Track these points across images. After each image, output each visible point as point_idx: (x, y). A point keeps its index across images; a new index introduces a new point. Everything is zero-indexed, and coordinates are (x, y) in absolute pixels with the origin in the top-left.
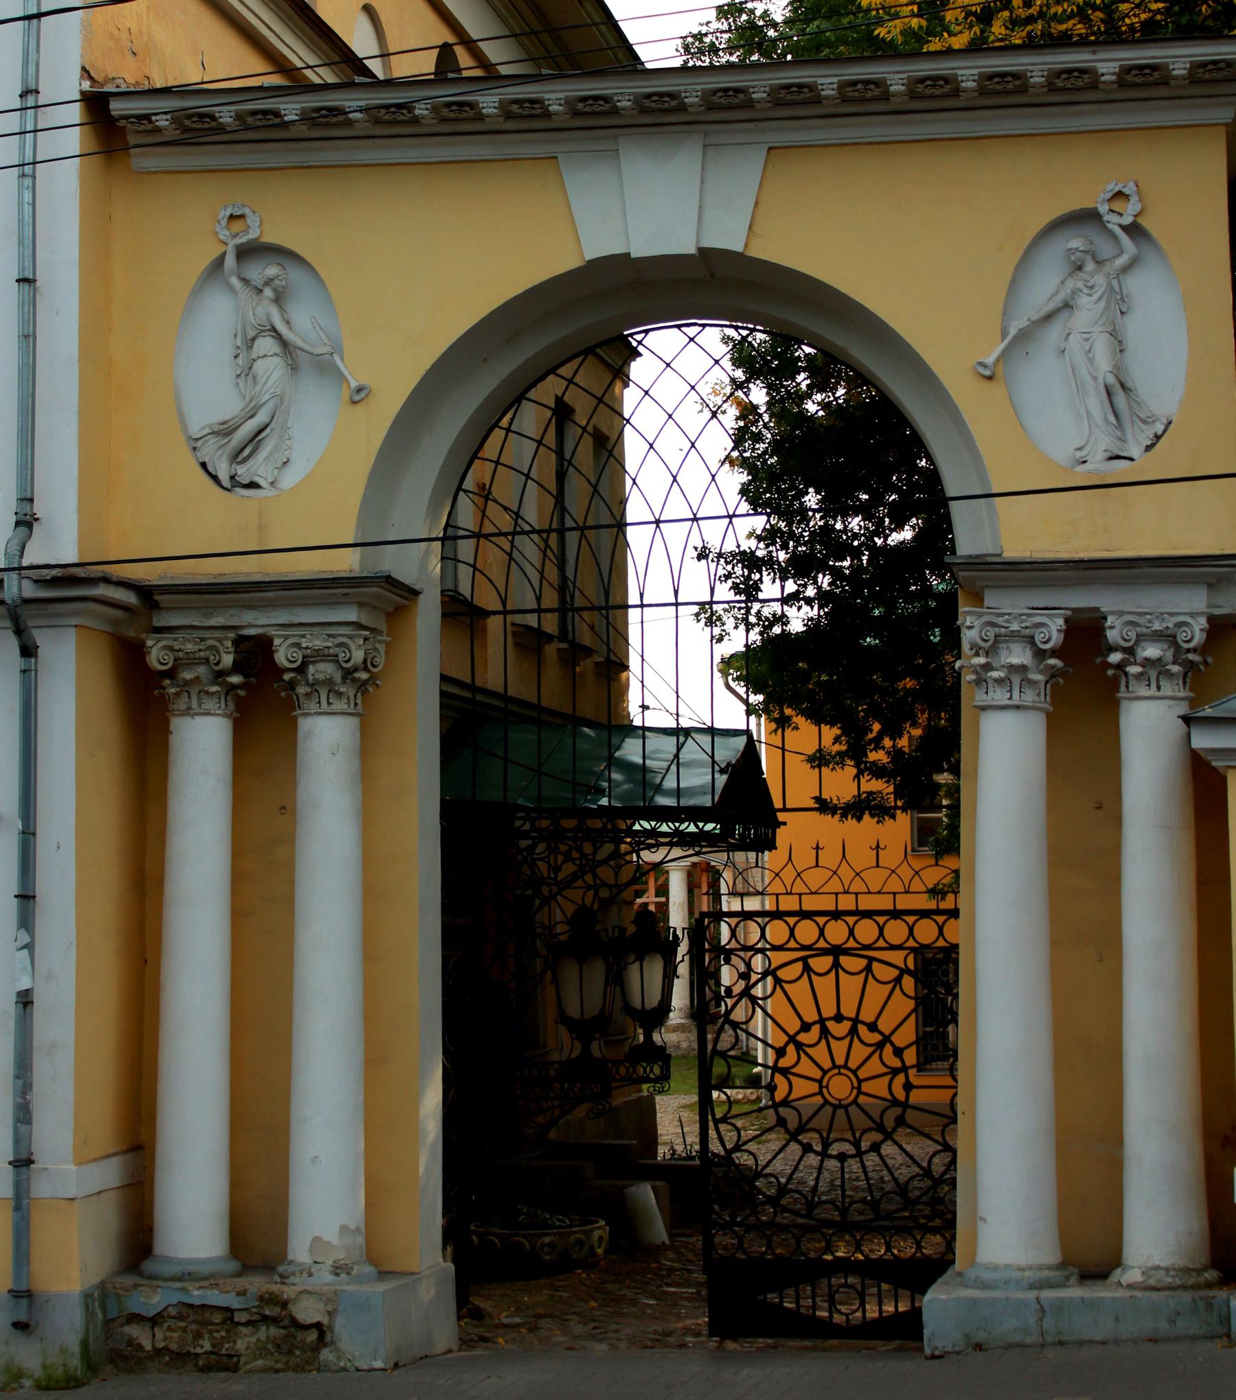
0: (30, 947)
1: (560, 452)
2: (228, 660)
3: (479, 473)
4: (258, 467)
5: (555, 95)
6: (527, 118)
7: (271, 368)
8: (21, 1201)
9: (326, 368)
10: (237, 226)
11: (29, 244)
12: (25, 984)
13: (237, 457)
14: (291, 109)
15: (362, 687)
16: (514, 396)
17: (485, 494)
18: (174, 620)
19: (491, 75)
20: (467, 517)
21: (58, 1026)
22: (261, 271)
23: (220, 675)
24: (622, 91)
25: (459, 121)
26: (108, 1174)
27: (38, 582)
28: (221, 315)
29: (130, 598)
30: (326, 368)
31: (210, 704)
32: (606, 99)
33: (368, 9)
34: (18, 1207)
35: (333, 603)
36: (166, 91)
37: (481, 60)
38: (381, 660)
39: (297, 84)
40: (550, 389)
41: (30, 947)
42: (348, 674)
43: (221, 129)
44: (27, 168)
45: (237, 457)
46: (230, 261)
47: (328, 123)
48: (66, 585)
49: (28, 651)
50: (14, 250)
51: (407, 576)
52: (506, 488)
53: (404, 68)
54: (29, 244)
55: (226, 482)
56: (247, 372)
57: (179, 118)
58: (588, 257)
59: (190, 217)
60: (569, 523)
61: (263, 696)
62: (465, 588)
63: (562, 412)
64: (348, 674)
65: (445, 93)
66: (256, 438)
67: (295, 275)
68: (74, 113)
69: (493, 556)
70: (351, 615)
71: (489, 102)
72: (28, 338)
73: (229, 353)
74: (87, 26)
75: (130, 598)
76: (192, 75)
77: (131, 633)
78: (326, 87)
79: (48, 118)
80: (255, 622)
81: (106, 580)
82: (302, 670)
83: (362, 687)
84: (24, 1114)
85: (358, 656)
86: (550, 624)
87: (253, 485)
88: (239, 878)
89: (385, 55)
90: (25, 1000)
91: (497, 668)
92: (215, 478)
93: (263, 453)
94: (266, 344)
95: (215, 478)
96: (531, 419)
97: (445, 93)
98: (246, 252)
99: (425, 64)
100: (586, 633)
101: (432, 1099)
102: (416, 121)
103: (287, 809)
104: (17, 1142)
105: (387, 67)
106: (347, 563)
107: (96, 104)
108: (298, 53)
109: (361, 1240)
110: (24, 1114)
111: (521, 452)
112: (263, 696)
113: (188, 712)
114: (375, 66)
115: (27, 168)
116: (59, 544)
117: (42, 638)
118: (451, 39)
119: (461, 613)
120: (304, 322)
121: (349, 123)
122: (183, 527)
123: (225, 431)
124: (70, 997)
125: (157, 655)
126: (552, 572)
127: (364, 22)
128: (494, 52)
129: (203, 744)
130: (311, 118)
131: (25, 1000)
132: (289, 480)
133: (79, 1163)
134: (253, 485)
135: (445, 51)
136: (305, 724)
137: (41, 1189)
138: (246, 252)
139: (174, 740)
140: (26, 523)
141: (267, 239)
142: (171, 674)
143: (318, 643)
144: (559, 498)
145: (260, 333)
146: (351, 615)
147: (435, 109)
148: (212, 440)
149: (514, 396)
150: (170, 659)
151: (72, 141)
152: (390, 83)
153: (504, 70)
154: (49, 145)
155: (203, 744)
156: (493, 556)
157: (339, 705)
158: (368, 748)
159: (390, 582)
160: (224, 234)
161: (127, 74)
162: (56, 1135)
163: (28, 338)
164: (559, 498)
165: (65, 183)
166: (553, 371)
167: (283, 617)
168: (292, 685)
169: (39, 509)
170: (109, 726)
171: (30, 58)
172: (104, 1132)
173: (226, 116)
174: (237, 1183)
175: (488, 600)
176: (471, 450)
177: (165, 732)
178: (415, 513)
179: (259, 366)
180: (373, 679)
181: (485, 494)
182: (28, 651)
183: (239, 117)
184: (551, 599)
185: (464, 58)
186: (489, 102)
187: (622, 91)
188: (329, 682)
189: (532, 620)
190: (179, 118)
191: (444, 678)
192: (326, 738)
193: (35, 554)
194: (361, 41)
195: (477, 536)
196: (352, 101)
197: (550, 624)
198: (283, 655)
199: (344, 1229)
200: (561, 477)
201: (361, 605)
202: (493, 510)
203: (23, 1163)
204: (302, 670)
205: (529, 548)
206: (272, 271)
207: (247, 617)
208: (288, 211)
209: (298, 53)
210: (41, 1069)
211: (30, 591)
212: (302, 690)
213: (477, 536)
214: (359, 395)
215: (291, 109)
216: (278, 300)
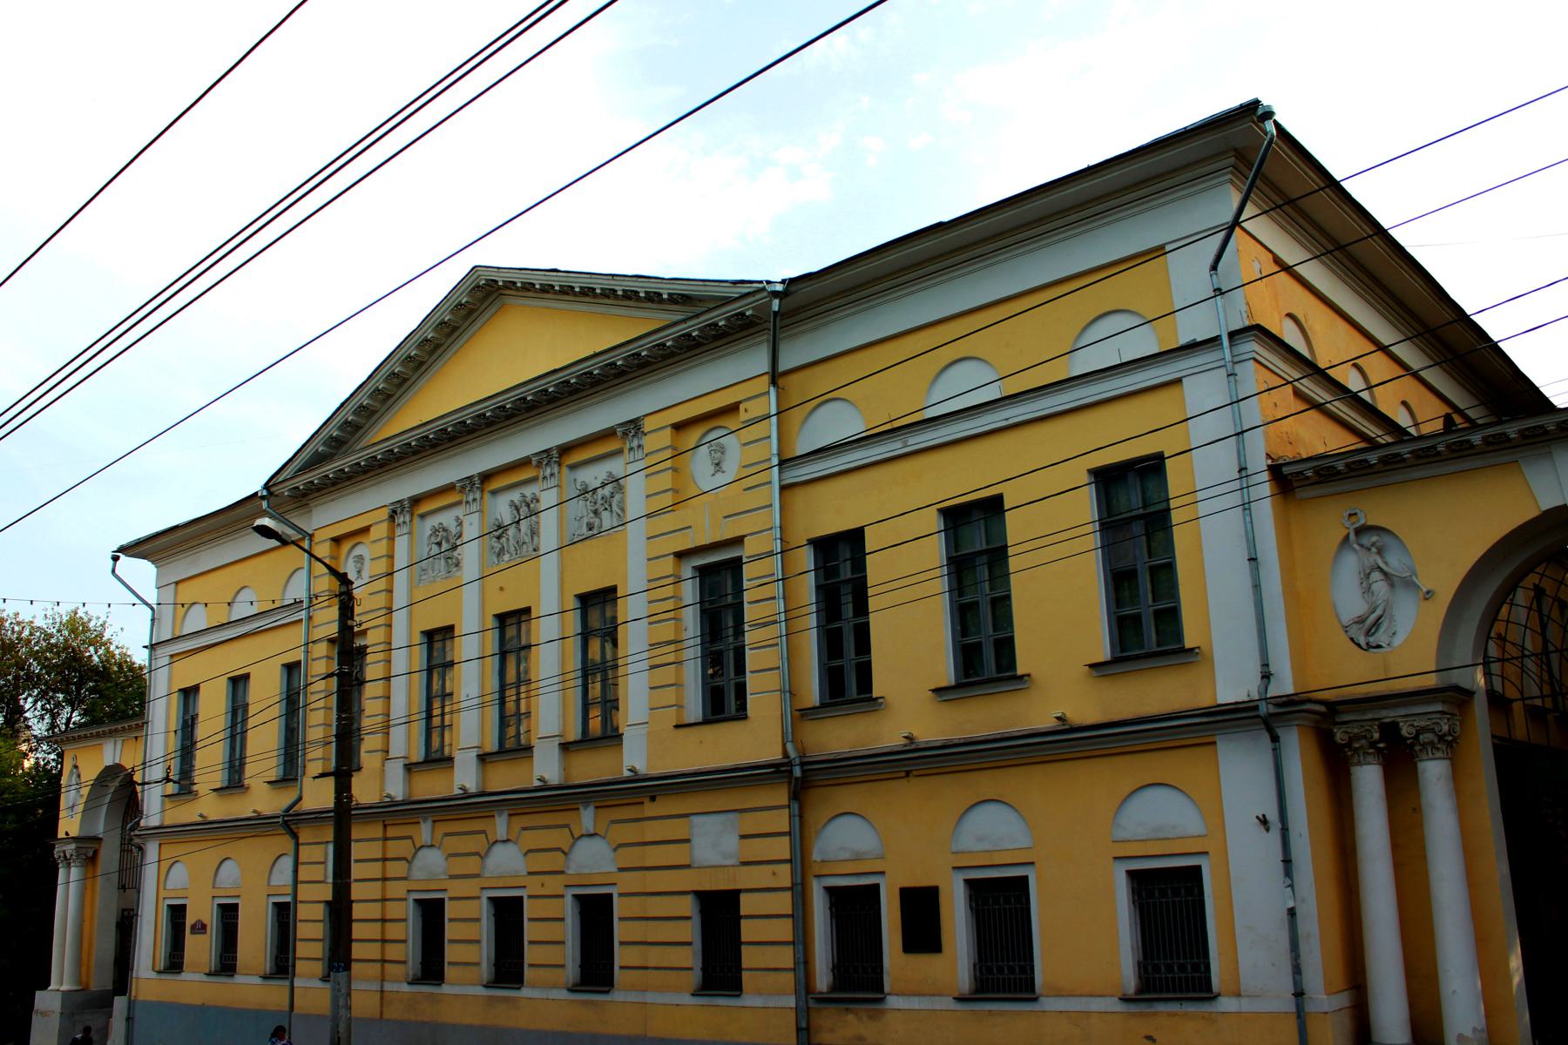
0: (1291, 886)
1: (1540, 611)
2: (1376, 736)
3: (1499, 627)
4: (1381, 637)
5: (1512, 430)
6: (1498, 444)
7: (1380, 587)
8: (1300, 1014)
9: (1409, 584)
10: (1353, 519)
11: (1251, 542)
12: (1291, 904)
13: (1368, 633)
14: (1373, 458)
15: (1449, 745)
16: (1505, 594)
17: (1502, 639)
18: (1347, 718)
19: (1473, 425)
20: (1493, 651)
21: (1310, 926)
22: (1367, 540)
23: (1373, 744)
24: (1549, 422)
25: (1462, 451)
26: (1343, 1000)
27: (1277, 705)
28: (1350, 565)
29: (1322, 709)
30: (1409, 584)
31: (1370, 759)
32: (1542, 427)
33: (1404, 403)
34: (1299, 1017)
35: (1428, 703)
36: (1310, 459)
37: (1467, 418)
38: (1458, 729)
39: (1373, 445)
40: (1532, 579)
41: (1291, 886)
42: (1441, 738)
43: (1339, 472)
44: (1246, 506)
45: (1368, 633)
46: (1352, 536)
47: (1392, 463)
48: (1290, 705)
49: (1275, 739)
50: (1245, 545)
51: (1467, 685)
52: (1514, 634)
53: (1426, 429)
54: (1251, 542)
55: (1363, 644)
56: (1368, 590)
57: (1317, 471)
58: (1544, 508)
59: (1328, 520)
60: (1551, 648)
61: (1399, 761)
62: (1498, 687)
63: (1539, 592)
64: (1441, 738)
65: (1452, 438)
66: (1377, 623)
67: (1386, 539)
68: (1265, 476)
69: (1511, 670)
70: (1439, 707)
71: (1476, 438)
72: (1257, 587)
73: (1356, 581)
74: (1266, 434)
75: (1322, 709)
76: (1321, 450)
77: (1324, 726)
78: (1388, 444)
79: (1253, 480)
80: (1388, 715)
81: (1310, 701)
82: (1416, 737)
83: (1450, 744)
84: (1297, 970)
85: (1446, 728)
86: (1549, 704)
87: (1379, 646)
88: (1396, 846)
89: (1416, 425)
90: (1292, 912)
91: (1521, 728)
92: (1359, 645)
93: (1382, 630)
94: (1376, 575)
95: (1359, 645)
96: (1521, 597)
97: (1452, 438)
98: (1360, 531)
99: (1438, 425)
100: (83, 879)
101: (1516, 963)
102: (1439, 453)
103: (1417, 810)
104: (1295, 983)
105: (1418, 430)
106: (1431, 681)
107: (1276, 471)
108: (1372, 430)
109: (1485, 1035)
110: (1297, 970)
111: (1521, 615)
112: (1399, 761)
113: (1359, 764)
114: (1412, 431)
115: (1246, 506)
116: (1285, 685)
117: (1280, 732)
118: (1449, 411)
119: (1497, 702)
120: (1394, 562)
121: (1404, 460)
122: (1346, 671)
123: (1361, 621)
124: (1315, 913)
125: (1340, 736)
126: (1546, 676)
127: (1403, 410)
128: (1471, 414)
129: (1369, 780)
130: (1384, 461)
131: (1292, 912)
132: (1397, 641)
133: (1328, 994)
134: (1379, 646)
135: (1448, 420)
136: (1422, 766)
137: (1310, 1007)
138: (1360, 531)
139: (1353, 778)
140: (1266, 676)
141: (1370, 523)
142: (1349, 745)
143: (1423, 724)
144: (1543, 634)
145: (1372, 570)
146: (1439, 707)
147: (1448, 446)
148: (1355, 627)
149: (1505, 594)
150: (1346, 737)
151: (1266, 489)
152: (1421, 438)
153: (1480, 422)
154: (1255, 493)
155: (1369, 780)
156: (1511, 670)
157: (1439, 754)
158: (1457, 777)
159: (1457, 689)
160: (1347, 524)
161: (1288, 453)
162: (1314, 979)
163: (1257, 587)
164: (1543, 634)
165: (1265, 510)
166: (1532, 571)
167: (1403, 712)
168: (1413, 745)
169: (1272, 669)
170: (1319, 772)
171: (1240, 453)
172: (1339, 980)
173: (1340, 466)
174: (1412, 1005)
175: (1512, 693)
176: (1491, 616)
177: (1348, 774)
178: (1465, 650)
179: (1374, 587)
180: (1455, 739)
181: (1502, 639)
182: (1275, 739)
183: (1347, 465)
184: (1546, 690)
185: (1457, 419)
186: (1476, 438)
187: (1549, 422)
188: (1432, 743)
189: (1538, 702)
190: (1317, 471)
191: (1493, 736)
192: (1434, 772)
193: (1273, 691)
194: (1403, 419)
195: (1499, 660)
196: (1404, 450)
197: (1549, 704)
198: (1405, 731)
199: (1475, 1029)
200: (1544, 626)
201: (1444, 702)
202: (1508, 647)
203: (1299, 994)
204: (1416, 737)
205: (1530, 664)
206: (1374, 539)
207: (1384, 713)
208: (1377, 509)
209: (1372, 430)
210: (1304, 948)
211: (1272, 709)
212: (1417, 748)
213: (1499, 660)
214: (1429, 595)
215: (1373, 458)
216: (1380, 552)
